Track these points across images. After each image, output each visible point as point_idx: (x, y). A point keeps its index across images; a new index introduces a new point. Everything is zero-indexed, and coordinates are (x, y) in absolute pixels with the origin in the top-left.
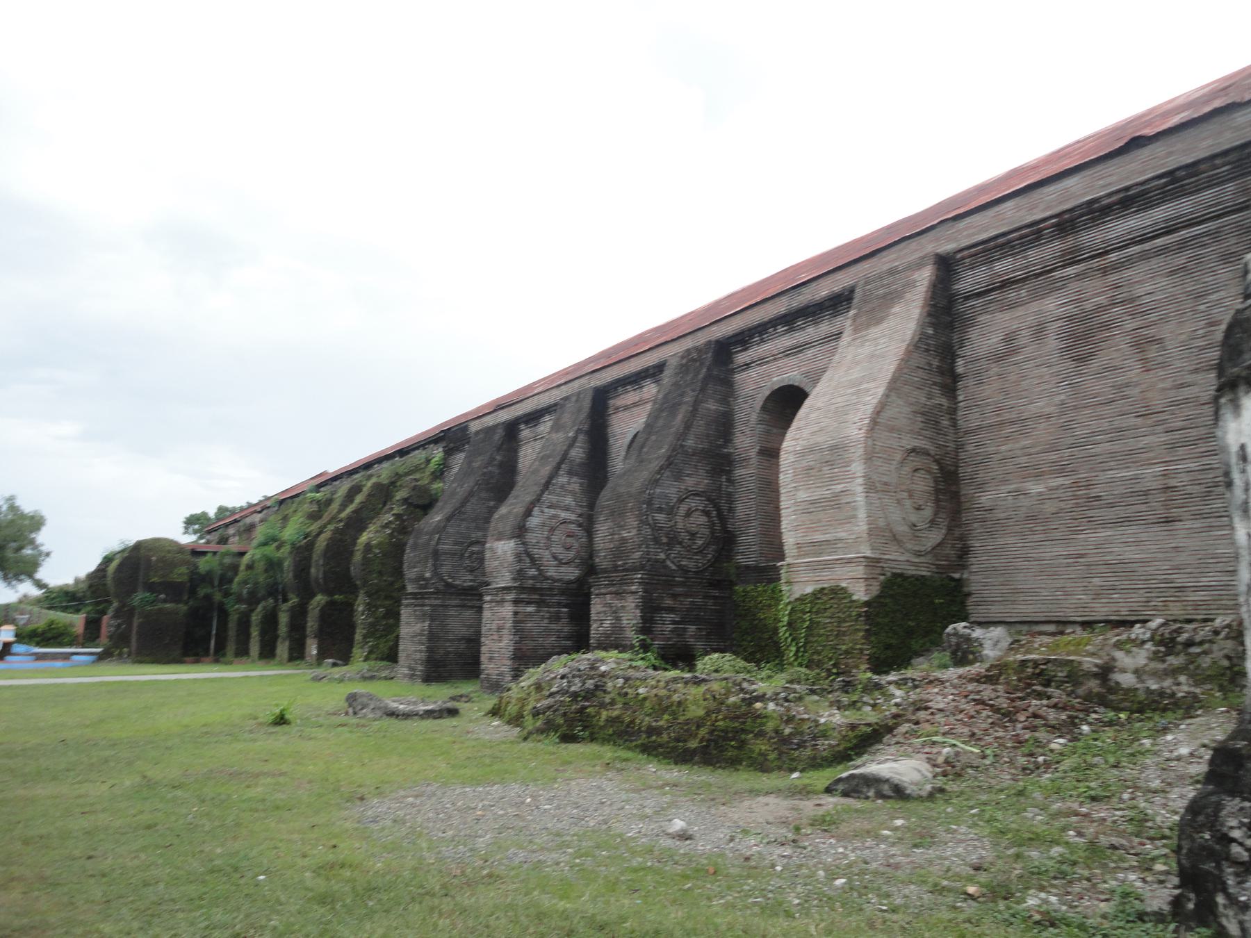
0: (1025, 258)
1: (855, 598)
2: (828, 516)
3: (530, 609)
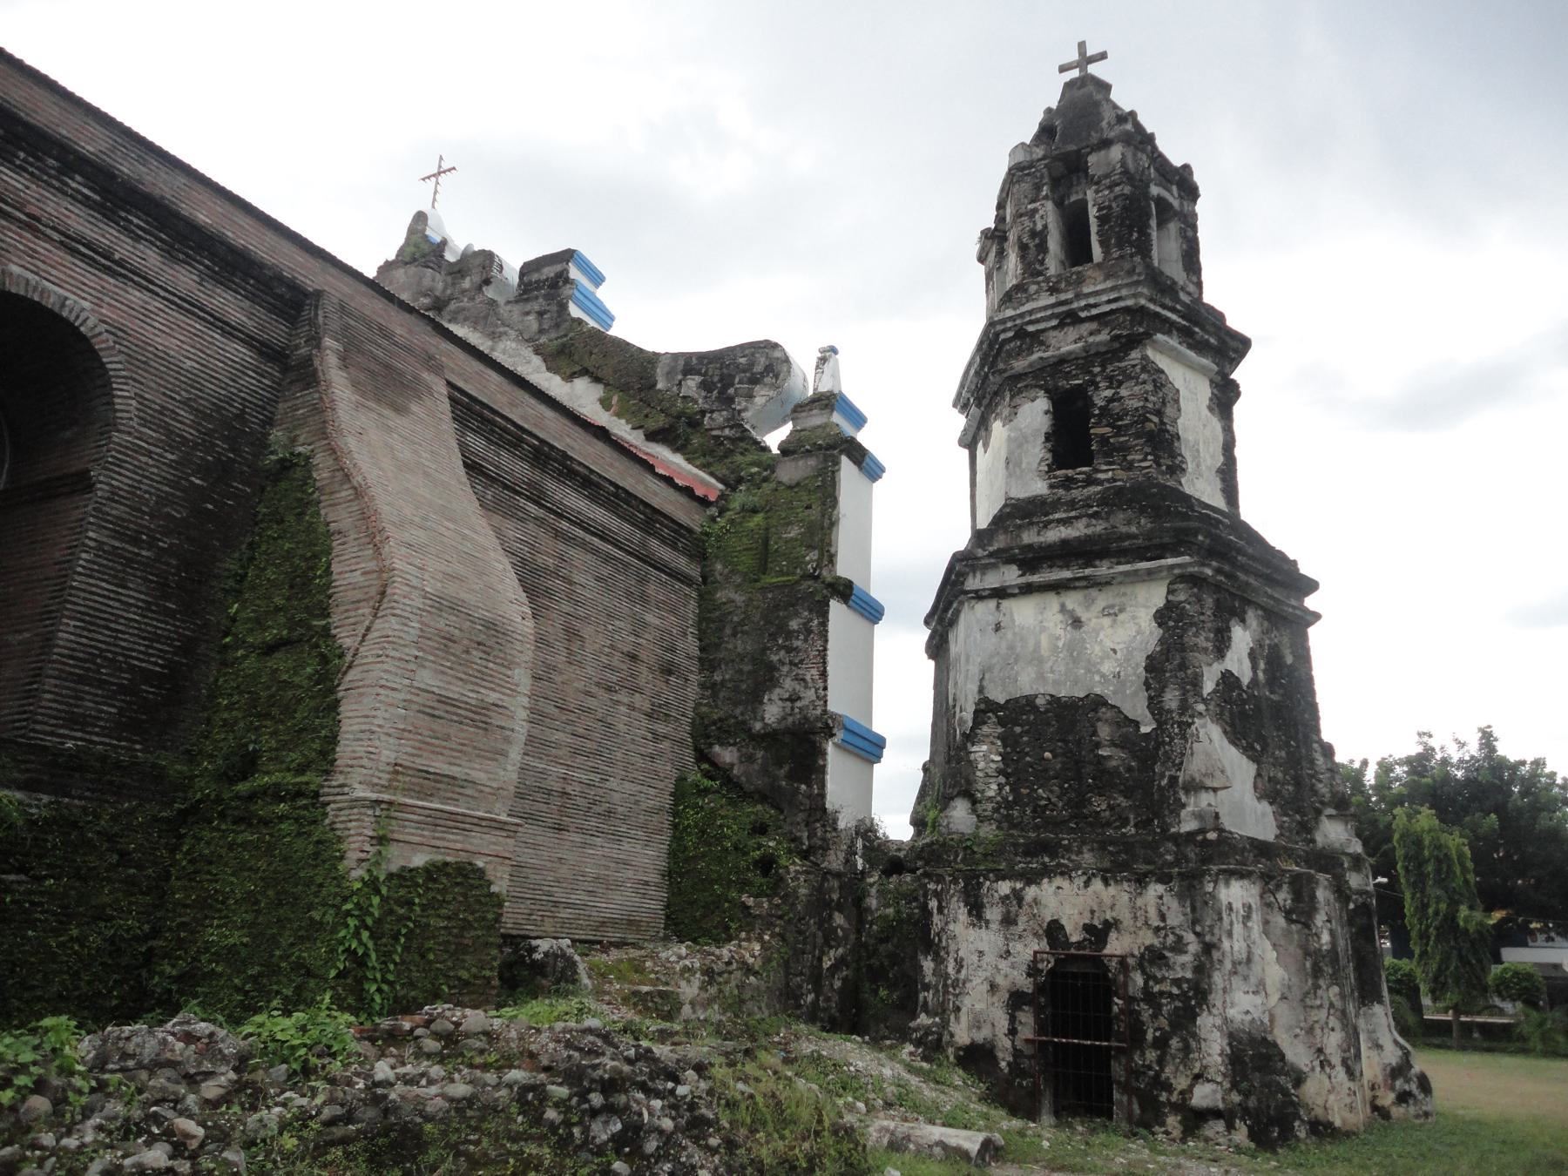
0: (498, 455)
1: (494, 889)
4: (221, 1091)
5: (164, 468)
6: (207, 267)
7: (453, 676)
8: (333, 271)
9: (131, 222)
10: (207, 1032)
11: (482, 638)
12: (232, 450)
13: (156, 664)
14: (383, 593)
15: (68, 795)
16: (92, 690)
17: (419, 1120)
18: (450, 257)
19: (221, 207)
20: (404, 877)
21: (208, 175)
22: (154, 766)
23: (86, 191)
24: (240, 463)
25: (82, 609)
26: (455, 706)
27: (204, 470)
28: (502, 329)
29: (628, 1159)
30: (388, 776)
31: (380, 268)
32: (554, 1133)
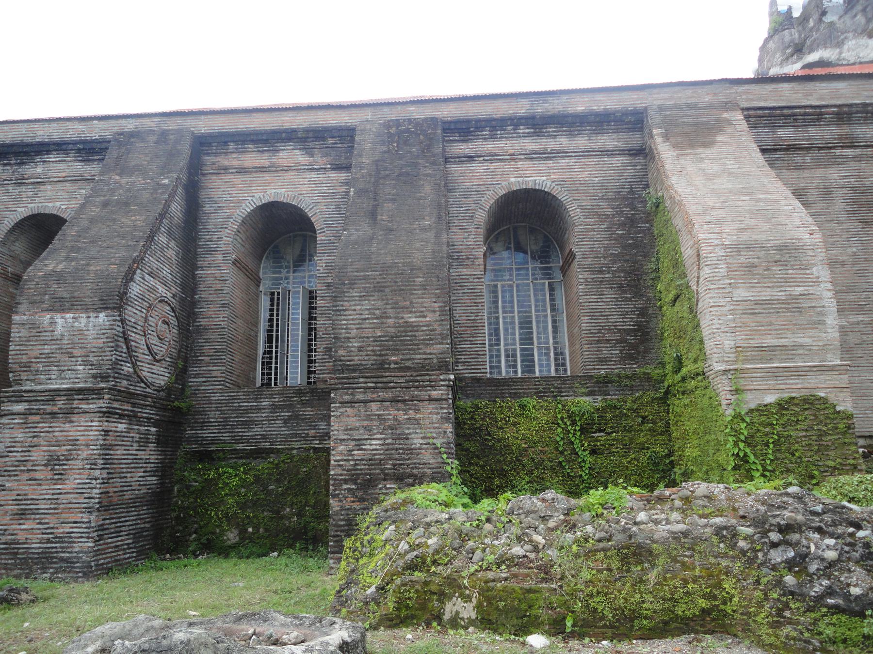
1: (838, 408)
2: (782, 319)
3: (122, 427)
4: (555, 524)
5: (602, 233)
6: (589, 130)
7: (761, 287)
8: (655, 91)
9: (549, 132)
10: (550, 498)
11: (777, 257)
12: (632, 210)
13: (630, 325)
14: (699, 255)
15: (609, 395)
16: (605, 345)
17: (648, 542)
18: (796, 14)
19: (586, 98)
20: (762, 410)
21: (567, 88)
22: (644, 373)
23: (527, 131)
24: (638, 214)
25: (589, 311)
26: (770, 304)
27: (622, 225)
28: (842, 37)
29: (797, 574)
30: (733, 355)
31: (760, 48)
32: (745, 555)
